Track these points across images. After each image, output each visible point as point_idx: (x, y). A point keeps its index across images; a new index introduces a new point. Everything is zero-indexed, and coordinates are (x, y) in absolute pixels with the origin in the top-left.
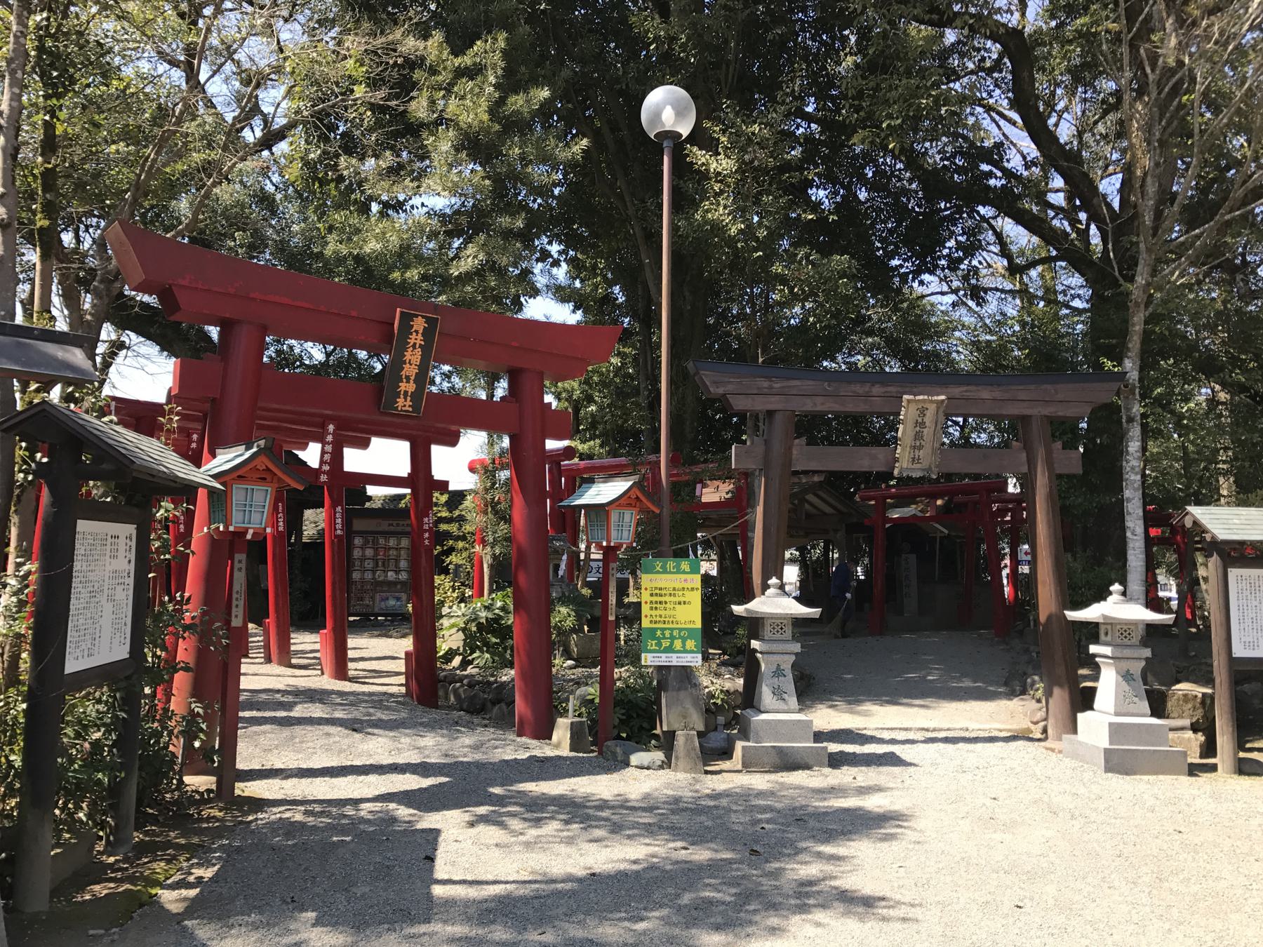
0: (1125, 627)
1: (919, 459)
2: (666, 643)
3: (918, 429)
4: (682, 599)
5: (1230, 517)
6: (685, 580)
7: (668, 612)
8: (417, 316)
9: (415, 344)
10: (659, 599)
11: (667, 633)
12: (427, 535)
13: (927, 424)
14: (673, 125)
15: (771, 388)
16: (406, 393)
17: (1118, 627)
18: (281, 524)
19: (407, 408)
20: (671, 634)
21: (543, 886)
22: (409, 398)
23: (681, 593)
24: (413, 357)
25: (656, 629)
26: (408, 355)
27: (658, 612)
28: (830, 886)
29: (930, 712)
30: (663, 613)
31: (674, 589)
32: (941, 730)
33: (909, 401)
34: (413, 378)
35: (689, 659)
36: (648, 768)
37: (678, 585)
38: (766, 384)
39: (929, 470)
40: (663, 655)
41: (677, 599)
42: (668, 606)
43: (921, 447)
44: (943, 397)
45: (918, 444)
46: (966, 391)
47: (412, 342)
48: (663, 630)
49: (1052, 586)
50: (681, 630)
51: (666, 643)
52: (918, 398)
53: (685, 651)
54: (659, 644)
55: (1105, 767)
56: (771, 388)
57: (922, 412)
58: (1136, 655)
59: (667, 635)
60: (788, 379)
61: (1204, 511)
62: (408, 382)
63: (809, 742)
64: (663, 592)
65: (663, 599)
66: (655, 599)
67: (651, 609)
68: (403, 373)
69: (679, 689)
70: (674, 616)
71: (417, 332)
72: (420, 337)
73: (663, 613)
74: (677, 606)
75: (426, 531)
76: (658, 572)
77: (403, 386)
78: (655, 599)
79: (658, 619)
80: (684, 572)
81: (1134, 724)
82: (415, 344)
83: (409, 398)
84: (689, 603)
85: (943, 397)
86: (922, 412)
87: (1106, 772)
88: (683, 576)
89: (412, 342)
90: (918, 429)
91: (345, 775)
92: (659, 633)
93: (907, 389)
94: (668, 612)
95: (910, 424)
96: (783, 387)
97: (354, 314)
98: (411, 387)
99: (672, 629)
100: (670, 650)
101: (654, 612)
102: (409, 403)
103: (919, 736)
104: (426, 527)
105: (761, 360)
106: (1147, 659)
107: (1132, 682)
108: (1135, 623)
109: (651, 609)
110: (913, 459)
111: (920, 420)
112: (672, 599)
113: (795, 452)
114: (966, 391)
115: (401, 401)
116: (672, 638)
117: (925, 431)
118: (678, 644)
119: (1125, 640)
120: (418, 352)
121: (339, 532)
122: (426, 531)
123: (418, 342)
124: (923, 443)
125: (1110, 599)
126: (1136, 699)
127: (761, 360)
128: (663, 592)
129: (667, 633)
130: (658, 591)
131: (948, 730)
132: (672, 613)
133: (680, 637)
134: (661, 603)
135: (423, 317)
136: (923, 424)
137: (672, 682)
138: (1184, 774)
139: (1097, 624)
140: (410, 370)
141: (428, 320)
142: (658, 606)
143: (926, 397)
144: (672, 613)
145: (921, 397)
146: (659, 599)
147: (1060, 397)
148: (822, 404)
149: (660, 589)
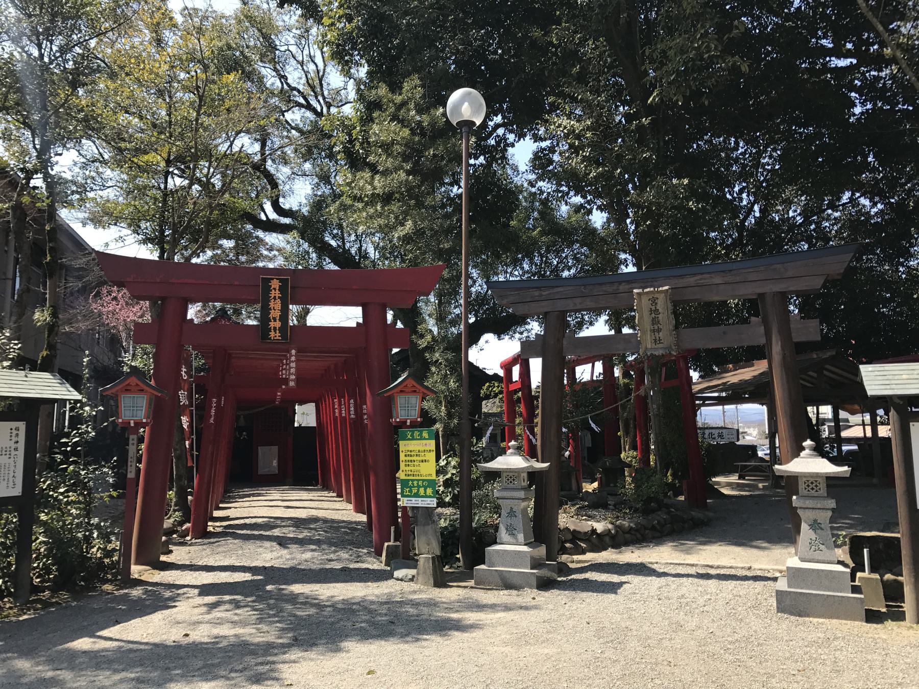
0: (812, 480)
1: (660, 340)
2: (415, 490)
3: (653, 315)
4: (424, 458)
5: (902, 372)
6: (426, 445)
7: (415, 468)
8: (273, 279)
9: (275, 297)
10: (410, 458)
11: (415, 483)
12: (365, 417)
13: (660, 310)
14: (470, 116)
15: (541, 295)
16: (275, 328)
17: (805, 479)
18: (343, 412)
19: (277, 338)
20: (418, 484)
21: (122, 644)
22: (278, 331)
23: (423, 454)
24: (275, 307)
25: (409, 480)
26: (272, 305)
27: (410, 468)
28: (56, 651)
29: (766, 552)
30: (412, 468)
31: (419, 451)
32: (724, 567)
33: (638, 294)
34: (278, 318)
35: (413, 502)
36: (401, 580)
37: (422, 449)
38: (537, 293)
39: (670, 348)
40: (413, 499)
41: (421, 458)
42: (416, 463)
43: (659, 330)
44: (667, 288)
45: (656, 328)
46: (701, 279)
47: (273, 296)
48: (413, 480)
49: (788, 443)
50: (423, 480)
51: (415, 490)
52: (646, 290)
53: (426, 496)
54: (411, 491)
55: (778, 608)
56: (541, 295)
57: (654, 301)
58: (819, 506)
59: (415, 485)
60: (682, 276)
61: (870, 369)
62: (275, 321)
63: (526, 568)
64: (412, 453)
65: (412, 458)
66: (408, 458)
67: (406, 465)
68: (271, 316)
69: (424, 525)
70: (419, 471)
71: (275, 289)
72: (277, 292)
73: (412, 468)
74: (421, 463)
75: (365, 414)
76: (409, 439)
77: (272, 324)
78: (408, 458)
79: (410, 473)
80: (425, 439)
81: (813, 570)
82: (275, 297)
83: (278, 331)
84: (428, 461)
85: (667, 288)
86: (654, 301)
87: (778, 612)
88: (424, 442)
89: (273, 296)
90: (653, 315)
91: (244, 572)
92: (410, 483)
93: (649, 284)
94: (415, 468)
95: (646, 313)
96: (548, 294)
97: (236, 283)
98: (278, 324)
99: (418, 480)
100: (417, 495)
101: (407, 468)
102: (278, 334)
103: (692, 571)
104: (365, 411)
105: (644, 268)
106: (833, 510)
107: (819, 531)
108: (817, 475)
109: (406, 465)
110: (655, 340)
111: (653, 308)
112: (418, 458)
113: (565, 343)
114: (701, 279)
115: (272, 334)
116: (419, 487)
117: (660, 316)
118: (422, 491)
119: (813, 492)
120: (279, 301)
121: (352, 416)
122: (365, 414)
123: (277, 295)
124: (661, 327)
125: (803, 454)
126: (822, 547)
127: (644, 268)
128: (412, 453)
129: (415, 483)
130: (409, 453)
131: (731, 567)
132: (418, 468)
133: (423, 486)
134: (411, 461)
135: (277, 279)
136: (656, 311)
137: (421, 519)
138: (861, 620)
139: (797, 476)
140: (275, 313)
141: (281, 280)
142: (410, 463)
143: (652, 289)
144: (418, 468)
145: (648, 290)
146: (410, 458)
147: (790, 274)
148: (580, 304)
149: (411, 451)
